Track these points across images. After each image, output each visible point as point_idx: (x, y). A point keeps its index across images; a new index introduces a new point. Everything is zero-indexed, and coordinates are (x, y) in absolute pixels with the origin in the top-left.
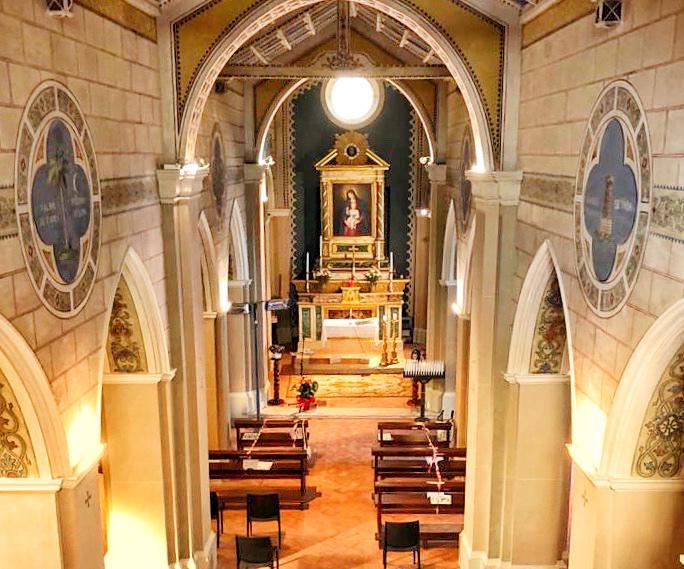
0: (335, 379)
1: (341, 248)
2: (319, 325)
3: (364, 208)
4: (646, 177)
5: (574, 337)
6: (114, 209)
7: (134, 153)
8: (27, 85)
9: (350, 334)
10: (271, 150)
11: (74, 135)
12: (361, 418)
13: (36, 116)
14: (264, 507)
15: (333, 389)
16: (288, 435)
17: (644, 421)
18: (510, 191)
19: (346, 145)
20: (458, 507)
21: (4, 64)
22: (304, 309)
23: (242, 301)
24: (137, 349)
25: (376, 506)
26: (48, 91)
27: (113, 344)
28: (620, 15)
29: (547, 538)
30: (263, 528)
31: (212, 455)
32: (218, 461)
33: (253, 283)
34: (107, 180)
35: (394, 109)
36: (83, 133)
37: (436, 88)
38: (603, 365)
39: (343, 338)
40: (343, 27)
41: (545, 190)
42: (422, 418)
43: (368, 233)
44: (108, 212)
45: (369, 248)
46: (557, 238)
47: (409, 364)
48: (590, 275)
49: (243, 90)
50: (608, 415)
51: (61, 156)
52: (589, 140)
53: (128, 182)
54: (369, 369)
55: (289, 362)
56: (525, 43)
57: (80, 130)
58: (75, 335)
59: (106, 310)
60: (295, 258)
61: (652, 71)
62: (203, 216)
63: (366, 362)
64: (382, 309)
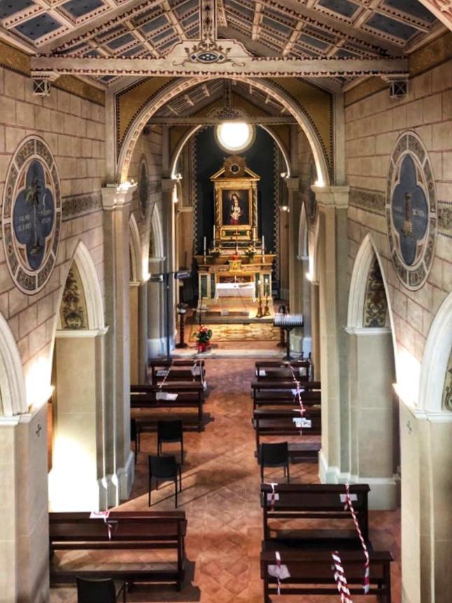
0: (224, 327)
1: (229, 233)
2: (213, 287)
3: (244, 205)
4: (432, 195)
5: (393, 303)
6: (70, 216)
7: (85, 178)
8: (14, 140)
9: (235, 294)
10: (180, 169)
11: (46, 169)
12: (245, 357)
13: (21, 159)
14: (172, 430)
15: (223, 335)
16: (190, 372)
17: (447, 367)
18: (341, 199)
19: (230, 164)
20: (316, 430)
21: (3, 127)
22: (202, 276)
23: (158, 273)
24: (82, 312)
25: (255, 428)
26: (30, 142)
27: (65, 308)
28: (406, 91)
29: (384, 456)
30: (171, 447)
31: (133, 389)
32: (137, 393)
33: (166, 259)
34: (67, 197)
35: (261, 139)
36: (52, 168)
37: (289, 130)
38: (415, 325)
39: (230, 297)
40: (228, 93)
41: (363, 197)
42: (288, 358)
43: (247, 223)
44: (66, 218)
45: (248, 233)
46: (375, 232)
47: (275, 316)
48: (400, 260)
49: (162, 131)
50: (421, 363)
51: (36, 184)
52: (392, 168)
53: (81, 197)
54: (249, 320)
55: (191, 314)
56: (346, 104)
57: (50, 166)
58: (37, 306)
59: (60, 286)
60: (196, 240)
61: (430, 126)
62: (132, 216)
63: (246, 314)
64: (258, 275)
